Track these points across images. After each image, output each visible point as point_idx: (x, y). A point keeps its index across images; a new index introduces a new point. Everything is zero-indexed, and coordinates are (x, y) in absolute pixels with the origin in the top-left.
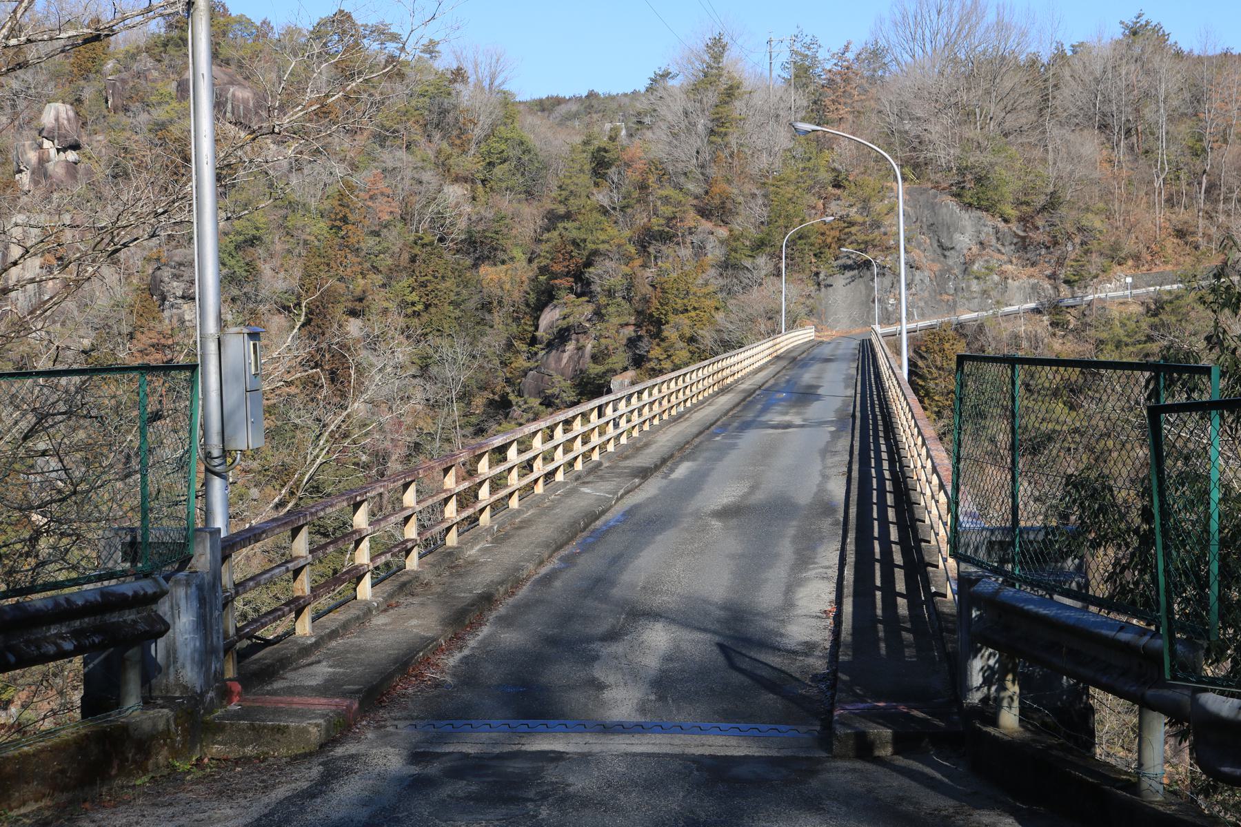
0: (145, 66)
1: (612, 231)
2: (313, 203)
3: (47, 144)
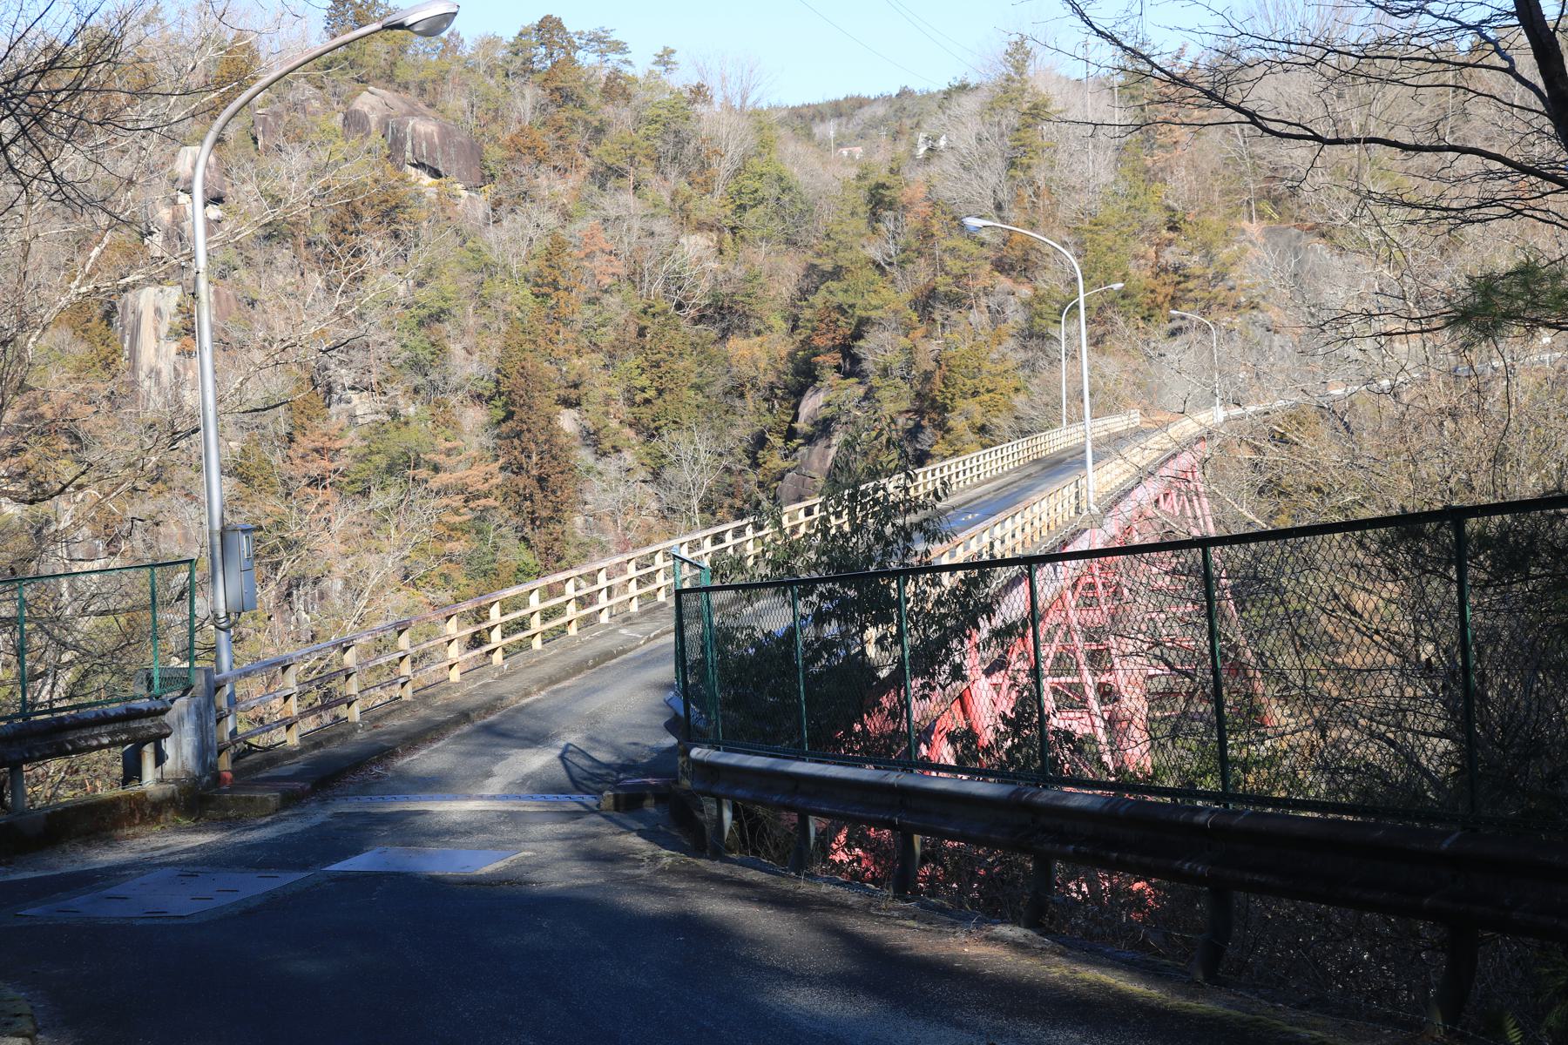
0: (303, 95)
1: (888, 294)
2: (515, 265)
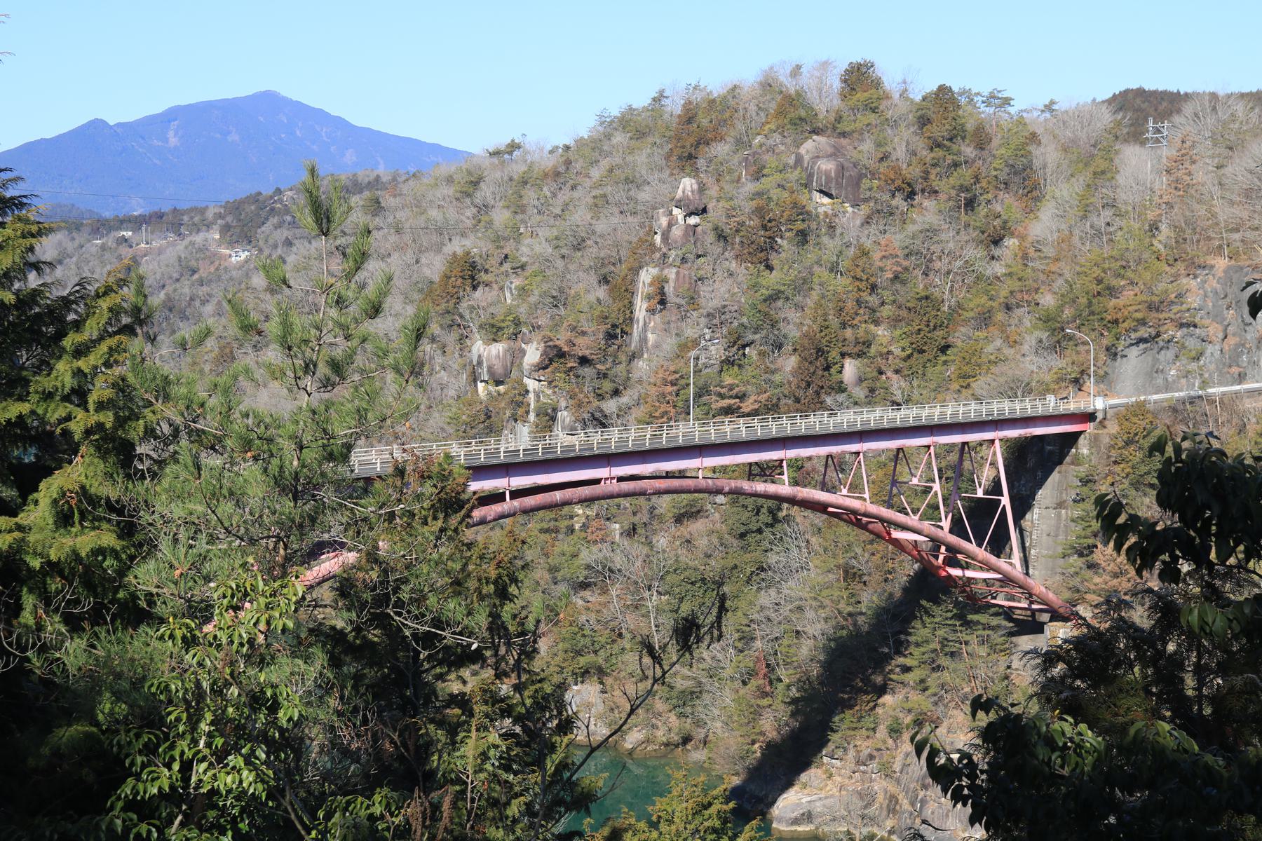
3: (676, 211)
